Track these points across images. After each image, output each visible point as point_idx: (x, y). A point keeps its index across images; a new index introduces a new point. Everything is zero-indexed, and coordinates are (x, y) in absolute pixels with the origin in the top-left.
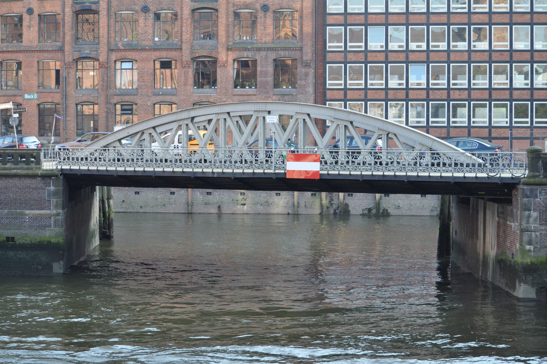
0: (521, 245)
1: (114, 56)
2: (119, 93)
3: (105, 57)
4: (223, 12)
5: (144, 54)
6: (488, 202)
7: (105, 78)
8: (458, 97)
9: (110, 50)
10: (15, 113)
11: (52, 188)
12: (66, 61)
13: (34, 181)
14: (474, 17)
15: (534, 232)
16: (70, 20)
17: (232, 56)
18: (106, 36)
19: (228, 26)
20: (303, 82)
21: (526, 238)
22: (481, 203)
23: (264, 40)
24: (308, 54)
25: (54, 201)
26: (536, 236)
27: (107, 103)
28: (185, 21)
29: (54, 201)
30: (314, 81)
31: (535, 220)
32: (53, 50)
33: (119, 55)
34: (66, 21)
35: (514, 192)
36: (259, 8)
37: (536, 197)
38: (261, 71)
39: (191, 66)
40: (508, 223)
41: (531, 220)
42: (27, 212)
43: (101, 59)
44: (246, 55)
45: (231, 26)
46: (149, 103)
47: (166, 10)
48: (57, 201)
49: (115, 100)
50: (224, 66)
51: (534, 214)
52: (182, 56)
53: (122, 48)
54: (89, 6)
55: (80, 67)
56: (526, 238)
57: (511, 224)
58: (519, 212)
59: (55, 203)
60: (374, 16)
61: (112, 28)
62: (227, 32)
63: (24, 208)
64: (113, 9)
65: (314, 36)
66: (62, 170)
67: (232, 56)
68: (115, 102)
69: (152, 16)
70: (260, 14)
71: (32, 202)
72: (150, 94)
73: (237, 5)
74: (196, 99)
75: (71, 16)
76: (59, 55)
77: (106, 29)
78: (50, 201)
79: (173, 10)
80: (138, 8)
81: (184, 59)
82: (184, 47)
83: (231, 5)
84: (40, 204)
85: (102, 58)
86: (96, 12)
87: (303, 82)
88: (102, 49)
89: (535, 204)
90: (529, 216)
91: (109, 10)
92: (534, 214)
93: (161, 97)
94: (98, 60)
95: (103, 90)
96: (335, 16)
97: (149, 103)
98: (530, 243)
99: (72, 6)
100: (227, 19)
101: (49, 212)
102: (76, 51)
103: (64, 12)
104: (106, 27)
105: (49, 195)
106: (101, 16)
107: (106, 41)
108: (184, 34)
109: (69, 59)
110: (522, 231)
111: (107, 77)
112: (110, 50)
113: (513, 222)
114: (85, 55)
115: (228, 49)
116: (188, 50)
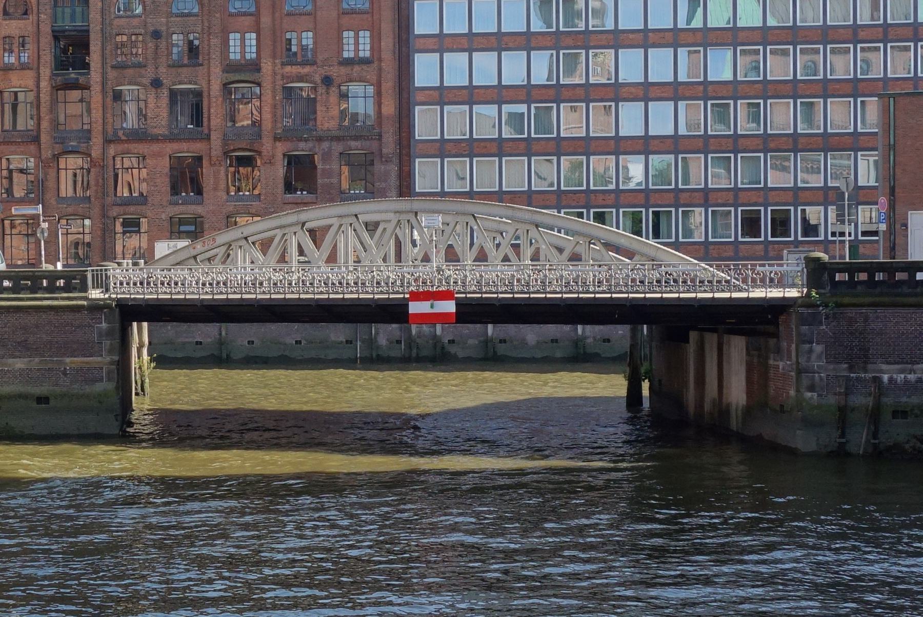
0: (798, 391)
1: (112, 150)
2: (119, 202)
3: (100, 151)
4: (269, 87)
5: (156, 147)
6: (726, 337)
7: (100, 180)
8: (601, 202)
9: (107, 141)
10: (44, 221)
11: (104, 325)
12: (43, 158)
13: (78, 315)
14: (624, 90)
15: (819, 373)
16: (48, 98)
17: (281, 148)
18: (101, 121)
19: (275, 106)
20: (384, 185)
21: (805, 382)
22: (711, 339)
23: (326, 125)
24: (389, 145)
25: (107, 343)
26: (821, 379)
27: (104, 215)
28: (214, 100)
29: (107, 343)
30: (398, 183)
31: (819, 357)
32: (23, 142)
33: (120, 147)
34: (42, 100)
35: (782, 318)
36: (319, 81)
37: (821, 323)
38: (323, 170)
39: (223, 163)
40: (771, 362)
41: (814, 356)
42: (68, 360)
43: (93, 155)
44: (303, 148)
45: (278, 107)
46: (163, 216)
47: (186, 84)
48: (111, 344)
49: (115, 211)
50: (270, 162)
51: (818, 348)
52: (210, 149)
53: (123, 138)
54: (77, 79)
55: (62, 166)
56: (805, 382)
57: (776, 363)
58: (794, 346)
59: (107, 347)
60: (483, 91)
61: (110, 111)
62: (274, 115)
63: (64, 355)
64: (109, 82)
65: (397, 120)
66: (119, 300)
67: (281, 148)
68: (115, 214)
69: (166, 93)
70: (321, 90)
71: (75, 346)
72: (165, 204)
73: (288, 77)
74: (231, 209)
75: (48, 93)
76: (32, 148)
77: (101, 112)
78: (101, 343)
79: (196, 84)
80: (146, 81)
81: (214, 153)
82: (214, 136)
83: (279, 77)
84: (86, 349)
85: (96, 152)
86: (86, 87)
87: (384, 185)
88: (94, 140)
89: (818, 334)
90: (811, 351)
91: (103, 84)
92: (818, 348)
93: (181, 207)
94: (90, 155)
95: (96, 198)
96: (427, 92)
97: (163, 216)
98: (811, 388)
99: (51, 79)
100: (274, 97)
101: (99, 359)
102: (57, 143)
103: (38, 87)
104: (101, 109)
105: (100, 335)
106: (93, 93)
107: (100, 128)
108: (212, 117)
109: (47, 154)
110: (799, 372)
111: (103, 179)
112: (107, 141)
113: (781, 360)
114: (70, 149)
115: (276, 139)
116: (219, 141)
